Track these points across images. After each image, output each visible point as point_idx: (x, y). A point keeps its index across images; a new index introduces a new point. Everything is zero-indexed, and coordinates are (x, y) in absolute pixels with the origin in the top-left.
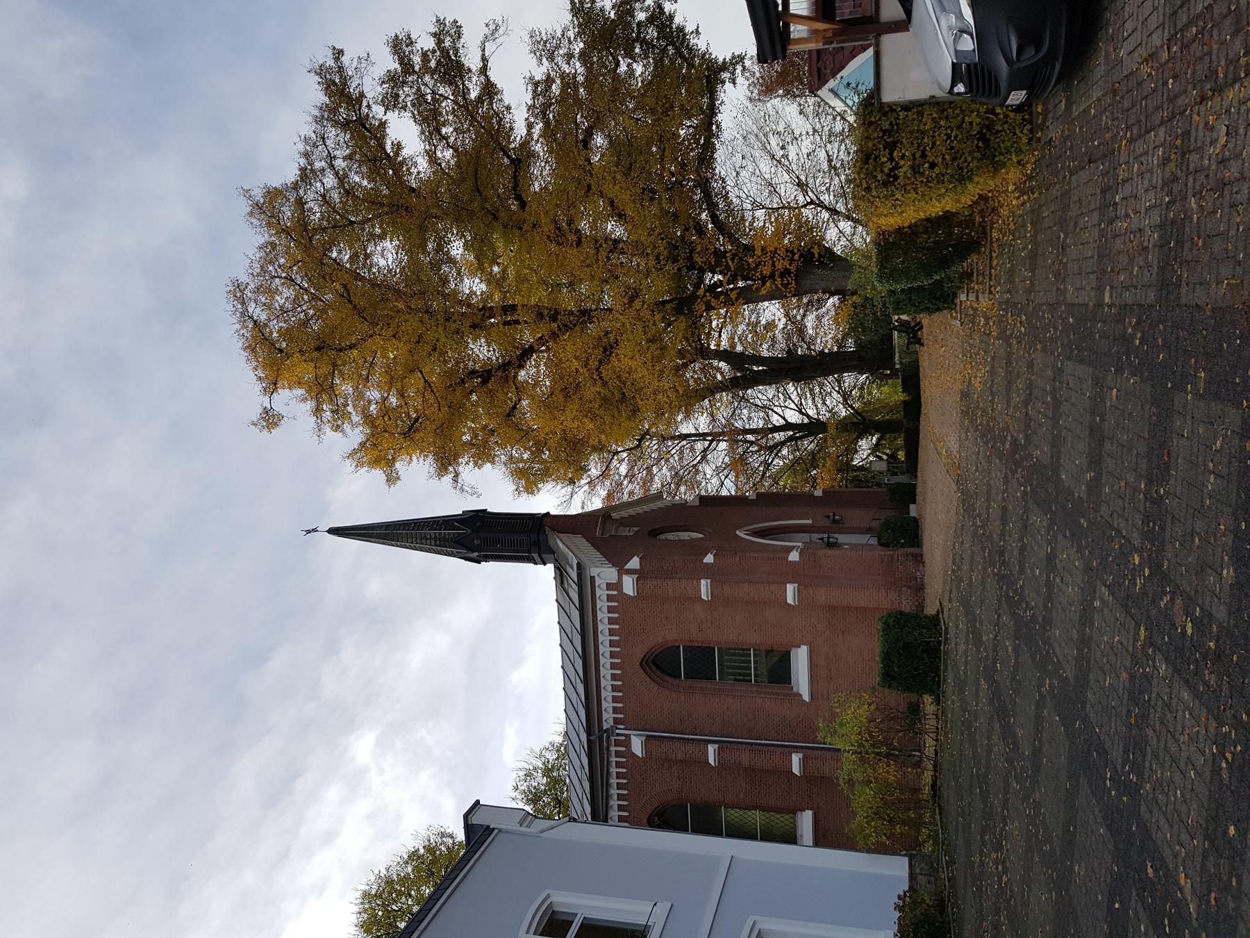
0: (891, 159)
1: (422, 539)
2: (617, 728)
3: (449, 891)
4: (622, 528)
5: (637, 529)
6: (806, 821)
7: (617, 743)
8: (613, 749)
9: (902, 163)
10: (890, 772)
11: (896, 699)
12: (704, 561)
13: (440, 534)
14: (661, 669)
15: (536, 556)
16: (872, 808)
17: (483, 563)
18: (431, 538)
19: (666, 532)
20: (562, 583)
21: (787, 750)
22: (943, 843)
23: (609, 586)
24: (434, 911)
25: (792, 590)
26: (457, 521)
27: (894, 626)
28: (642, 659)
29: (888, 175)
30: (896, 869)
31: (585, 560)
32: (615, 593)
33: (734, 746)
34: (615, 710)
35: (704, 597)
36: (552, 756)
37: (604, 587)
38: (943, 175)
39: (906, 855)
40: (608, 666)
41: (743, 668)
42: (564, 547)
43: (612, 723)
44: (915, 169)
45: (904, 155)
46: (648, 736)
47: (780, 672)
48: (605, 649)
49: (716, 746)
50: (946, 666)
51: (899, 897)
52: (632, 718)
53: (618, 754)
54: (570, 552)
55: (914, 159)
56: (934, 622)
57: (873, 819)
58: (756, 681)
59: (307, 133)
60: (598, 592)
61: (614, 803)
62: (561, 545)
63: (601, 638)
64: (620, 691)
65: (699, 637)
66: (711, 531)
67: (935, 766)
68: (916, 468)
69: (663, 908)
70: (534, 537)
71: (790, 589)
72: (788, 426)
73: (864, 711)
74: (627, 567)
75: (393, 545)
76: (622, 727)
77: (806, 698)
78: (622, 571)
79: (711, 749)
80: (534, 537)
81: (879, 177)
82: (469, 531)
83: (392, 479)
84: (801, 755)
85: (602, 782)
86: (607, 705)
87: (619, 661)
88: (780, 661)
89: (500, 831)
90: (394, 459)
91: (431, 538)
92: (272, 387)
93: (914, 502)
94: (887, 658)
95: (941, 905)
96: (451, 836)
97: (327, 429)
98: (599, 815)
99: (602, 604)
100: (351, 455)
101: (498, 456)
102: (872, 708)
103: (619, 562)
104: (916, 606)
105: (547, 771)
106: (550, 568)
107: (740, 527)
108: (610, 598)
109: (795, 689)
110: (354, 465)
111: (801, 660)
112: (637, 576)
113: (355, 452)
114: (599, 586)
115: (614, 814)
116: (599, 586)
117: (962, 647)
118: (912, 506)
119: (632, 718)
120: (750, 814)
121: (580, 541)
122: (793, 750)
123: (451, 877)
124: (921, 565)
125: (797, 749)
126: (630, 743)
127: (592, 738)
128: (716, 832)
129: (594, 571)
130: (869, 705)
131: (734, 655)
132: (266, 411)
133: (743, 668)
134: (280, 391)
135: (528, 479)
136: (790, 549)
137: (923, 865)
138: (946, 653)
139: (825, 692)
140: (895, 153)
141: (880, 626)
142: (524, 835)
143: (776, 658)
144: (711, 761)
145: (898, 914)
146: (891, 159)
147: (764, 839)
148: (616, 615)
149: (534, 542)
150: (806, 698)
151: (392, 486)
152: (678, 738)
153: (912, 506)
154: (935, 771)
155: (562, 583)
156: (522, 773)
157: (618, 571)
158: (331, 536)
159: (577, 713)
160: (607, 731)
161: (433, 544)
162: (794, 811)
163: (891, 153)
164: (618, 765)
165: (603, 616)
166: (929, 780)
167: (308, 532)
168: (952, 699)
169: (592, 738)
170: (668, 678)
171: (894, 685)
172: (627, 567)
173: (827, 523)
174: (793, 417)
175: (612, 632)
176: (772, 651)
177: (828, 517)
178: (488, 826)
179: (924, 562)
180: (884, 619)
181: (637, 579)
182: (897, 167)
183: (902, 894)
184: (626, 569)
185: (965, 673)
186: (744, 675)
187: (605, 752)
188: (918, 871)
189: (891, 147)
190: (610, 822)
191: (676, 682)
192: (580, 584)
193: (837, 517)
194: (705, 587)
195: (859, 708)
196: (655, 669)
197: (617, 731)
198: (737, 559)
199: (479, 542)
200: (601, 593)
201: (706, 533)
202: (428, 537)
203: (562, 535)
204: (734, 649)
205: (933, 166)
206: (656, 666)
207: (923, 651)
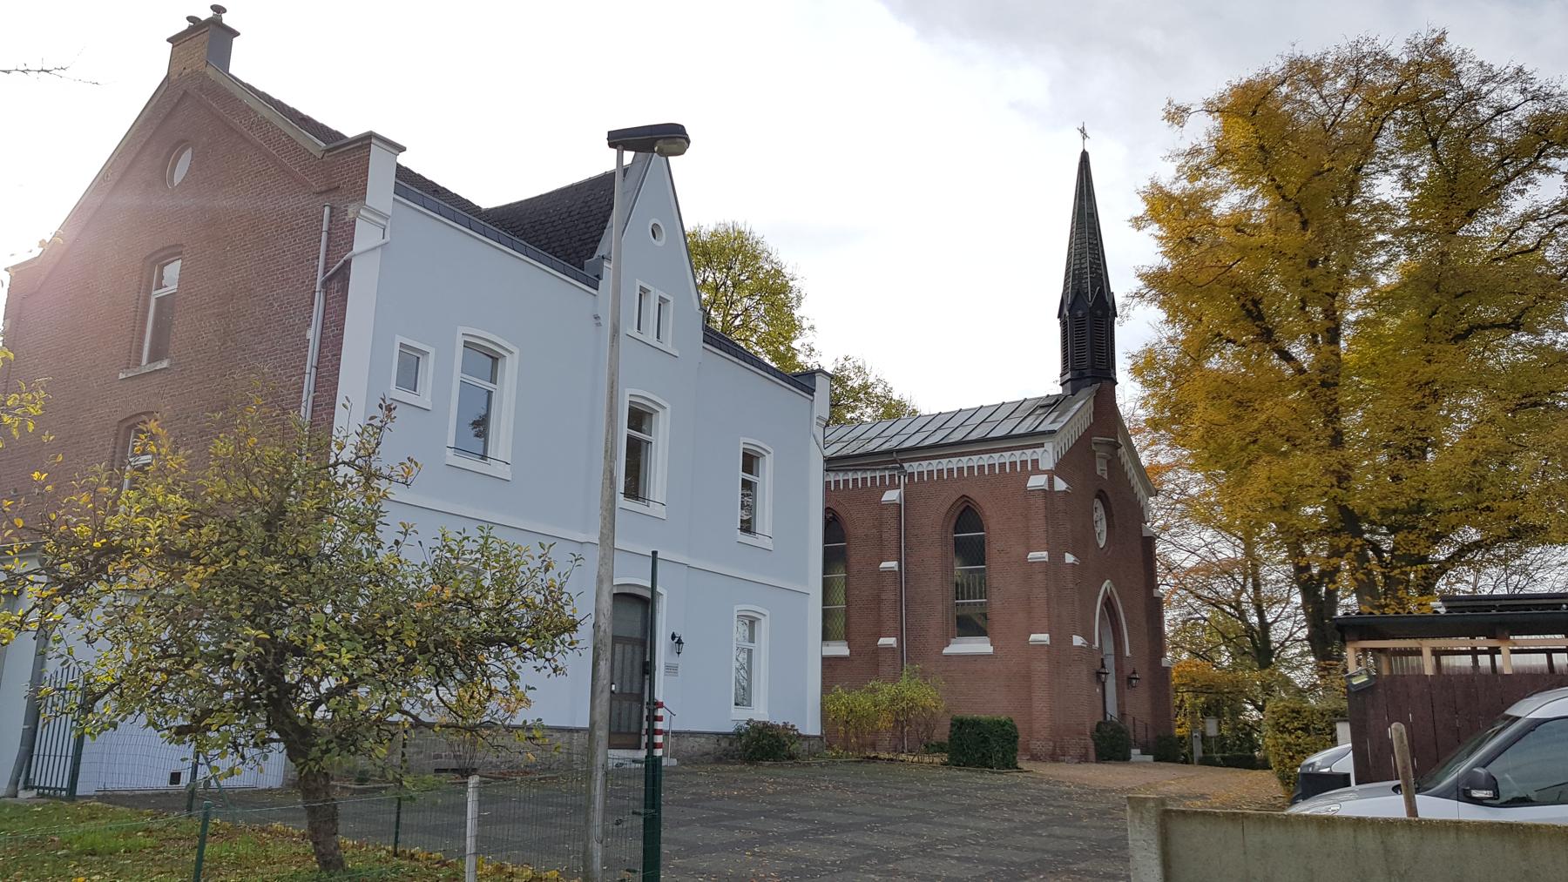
0: (1296, 729)
2: (905, 476)
3: (766, 375)
4: (1105, 462)
5: (1106, 477)
6: (840, 649)
8: (887, 473)
11: (942, 733)
12: (1066, 554)
15: (1068, 376)
16: (855, 707)
17: (1058, 321)
18: (1081, 264)
19: (1104, 505)
21: (899, 633)
22: (834, 762)
23: (1035, 462)
24: (752, 368)
25: (1043, 639)
26: (1101, 291)
27: (1003, 730)
28: (967, 497)
29: (1283, 726)
30: (811, 725)
31: (1058, 438)
32: (1029, 468)
33: (898, 585)
34: (921, 474)
35: (1031, 555)
36: (879, 390)
38: (1284, 765)
39: (822, 733)
40: (960, 465)
41: (969, 592)
42: (1075, 411)
44: (1288, 746)
45: (1300, 738)
46: (900, 505)
47: (969, 626)
48: (975, 461)
49: (896, 569)
50: (972, 771)
51: (793, 726)
54: (1068, 418)
55: (1296, 745)
56: (1010, 764)
57: (846, 708)
58: (957, 604)
59: (1537, 80)
60: (1029, 452)
61: (841, 477)
62: (1077, 406)
63: (985, 457)
65: (992, 550)
67: (892, 760)
69: (768, 544)
70: (1088, 373)
71: (1044, 638)
72: (1265, 627)
73: (930, 702)
74: (1056, 478)
76: (907, 481)
77: (946, 651)
78: (1051, 474)
79: (893, 564)
81: (1282, 720)
82: (1091, 304)
83: (1137, 223)
85: (867, 464)
86: (925, 466)
87: (966, 475)
88: (978, 626)
89: (812, 401)
90: (1158, 221)
91: (1081, 264)
92: (1210, 108)
93: (1155, 761)
94: (976, 723)
95: (791, 757)
97: (1181, 161)
98: (832, 464)
99: (1017, 456)
102: (934, 709)
103: (1060, 469)
104: (1036, 754)
105: (865, 387)
106: (1058, 390)
107: (1115, 583)
108: (1024, 463)
109: (953, 640)
110: (1145, 189)
111: (979, 646)
112: (1047, 488)
113: (1160, 189)
114: (1035, 452)
115: (832, 477)
116: (1035, 452)
118: (1138, 751)
120: (840, 595)
121: (1085, 421)
122: (899, 638)
123: (777, 373)
124: (1077, 761)
125: (900, 642)
126: (894, 489)
127: (894, 455)
128: (826, 569)
129: (1049, 446)
130: (936, 707)
131: (980, 584)
133: (969, 592)
134: (1211, 117)
136: (1088, 636)
137: (816, 747)
138: (982, 772)
139: (953, 669)
140: (1299, 731)
141: (1003, 718)
142: (811, 419)
143: (980, 623)
144: (883, 565)
145: (781, 724)
146: (1296, 729)
147: (824, 610)
148: (1008, 470)
149: (1083, 373)
150: (946, 651)
151: (1131, 224)
152: (901, 534)
154: (888, 760)
155: (1042, 407)
157: (1052, 470)
159: (917, 432)
160: (902, 467)
161: (1076, 267)
162: (848, 638)
163: (1299, 729)
164: (874, 479)
165: (1007, 457)
167: (1082, 131)
168: (943, 772)
169: (894, 455)
170: (954, 521)
171: (954, 729)
172: (1056, 479)
173: (1128, 671)
175: (992, 466)
177: (1134, 673)
178: (814, 391)
179: (1079, 763)
180: (1009, 722)
182: (1290, 733)
183: (796, 728)
184: (1053, 478)
185: (959, 781)
186: (962, 593)
189: (1305, 729)
190: (826, 473)
191: (951, 529)
192: (1032, 434)
194: (1041, 555)
195: (933, 698)
196: (961, 509)
197: (902, 477)
198: (1071, 586)
199: (1080, 316)
200: (1028, 455)
201: (1106, 548)
202: (1083, 261)
203: (1091, 402)
204: (985, 584)
206: (964, 510)
207: (983, 754)
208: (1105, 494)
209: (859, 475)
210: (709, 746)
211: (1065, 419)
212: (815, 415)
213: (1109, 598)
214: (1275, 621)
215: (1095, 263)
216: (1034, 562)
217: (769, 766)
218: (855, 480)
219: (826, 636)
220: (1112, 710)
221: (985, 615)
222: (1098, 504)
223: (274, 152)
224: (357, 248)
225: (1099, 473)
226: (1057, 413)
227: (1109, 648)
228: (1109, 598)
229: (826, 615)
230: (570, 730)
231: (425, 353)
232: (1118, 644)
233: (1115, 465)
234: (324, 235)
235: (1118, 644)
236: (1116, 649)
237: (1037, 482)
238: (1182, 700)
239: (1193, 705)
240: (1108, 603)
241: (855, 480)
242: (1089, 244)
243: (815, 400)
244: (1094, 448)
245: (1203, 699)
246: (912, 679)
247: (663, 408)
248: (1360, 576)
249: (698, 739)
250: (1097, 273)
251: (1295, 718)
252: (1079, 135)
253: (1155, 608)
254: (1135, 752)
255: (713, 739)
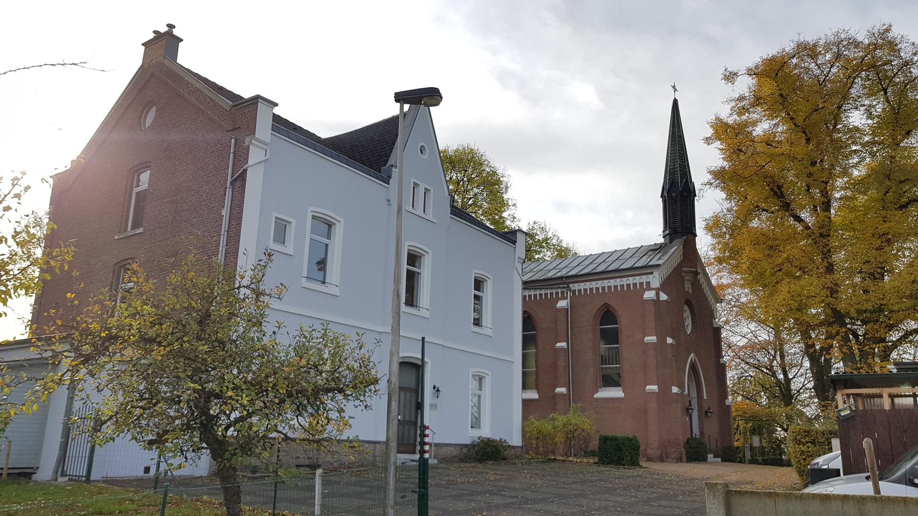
0: (807, 442)
1: (674, 160)
3: (488, 233)
4: (690, 283)
5: (691, 292)
6: (533, 395)
7: (563, 293)
8: (559, 290)
9: (806, 447)
10: (560, 438)
11: (594, 444)
12: (668, 338)
13: (677, 171)
14: (604, 314)
15: (667, 232)
18: (674, 165)
19: (690, 308)
20: (652, 250)
24: (480, 229)
29: (800, 441)
30: (516, 440)
31: (662, 269)
32: (645, 287)
34: (580, 291)
35: (646, 338)
36: (554, 242)
37: (648, 280)
41: (609, 361)
43: (573, 289)
44: (803, 452)
46: (568, 309)
47: (610, 381)
49: (566, 347)
51: (505, 440)
52: (576, 299)
53: (557, 293)
58: (602, 368)
62: (673, 250)
63: (618, 280)
64: (590, 292)
65: (623, 336)
66: (693, 338)
67: (564, 460)
68: (766, 464)
70: (679, 230)
71: (655, 388)
72: (788, 381)
73: (587, 426)
75: (668, 145)
77: (596, 396)
79: (563, 344)
80: (679, 230)
81: (798, 437)
83: (708, 141)
84: (566, 393)
86: (582, 286)
88: (615, 381)
89: (515, 248)
90: (720, 140)
92: (750, 72)
93: (714, 457)
96: (506, 192)
97: (733, 104)
98: (527, 285)
99: (638, 280)
100: (717, 118)
101: (731, 202)
103: (664, 287)
105: (546, 240)
106: (661, 240)
108: (641, 284)
109: (600, 389)
111: (616, 393)
115: (527, 293)
117: (617, 473)
118: (712, 455)
119: (576, 299)
121: (678, 259)
125: (569, 391)
129: (656, 274)
130: (590, 429)
131: (616, 356)
132: (735, 74)
133: (609, 361)
134: (750, 78)
135: (714, 226)
136: (681, 386)
137: (519, 453)
141: (631, 436)
142: (514, 260)
143: (616, 379)
145: (498, 439)
146: (807, 442)
150: (596, 396)
153: (712, 455)
155: (652, 250)
156: (543, 225)
157: (658, 288)
158: (672, 102)
162: (537, 388)
165: (631, 280)
166: (558, 458)
167: (674, 87)
170: (600, 318)
172: (661, 293)
173: (705, 408)
174: (794, 386)
176: (620, 377)
177: (709, 409)
181: (654, 300)
182: (804, 445)
187: (557, 286)
188: (517, 450)
189: (813, 442)
193: (709, 414)
197: (569, 293)
198: (671, 357)
200: (644, 279)
205: (805, 460)
206: (606, 312)
207: (619, 457)
208: (690, 302)
209: (543, 292)
210: (456, 452)
211: (666, 257)
212: (517, 256)
213: (693, 364)
214: (794, 378)
215: (683, 165)
216: (648, 343)
217: (491, 464)
218: (541, 295)
219: (525, 387)
220: (696, 430)
221: (619, 375)
222: (686, 308)
223: (203, 108)
224: (250, 163)
225: (686, 289)
226: (661, 254)
227: (694, 394)
228: (693, 364)
229: (524, 374)
230: (375, 443)
231: (290, 223)
232: (700, 392)
233: (696, 284)
234: (232, 155)
235: (700, 392)
236: (698, 393)
237: (649, 295)
238: (738, 425)
239: (745, 428)
240: (693, 367)
241: (541, 295)
242: (679, 153)
243: (517, 248)
244: (683, 274)
245: (751, 424)
246: (576, 412)
247: (428, 253)
248: (844, 350)
249: (449, 448)
250: (684, 171)
251: (806, 435)
252: (672, 90)
253: (721, 370)
254: (710, 456)
255: (458, 448)
